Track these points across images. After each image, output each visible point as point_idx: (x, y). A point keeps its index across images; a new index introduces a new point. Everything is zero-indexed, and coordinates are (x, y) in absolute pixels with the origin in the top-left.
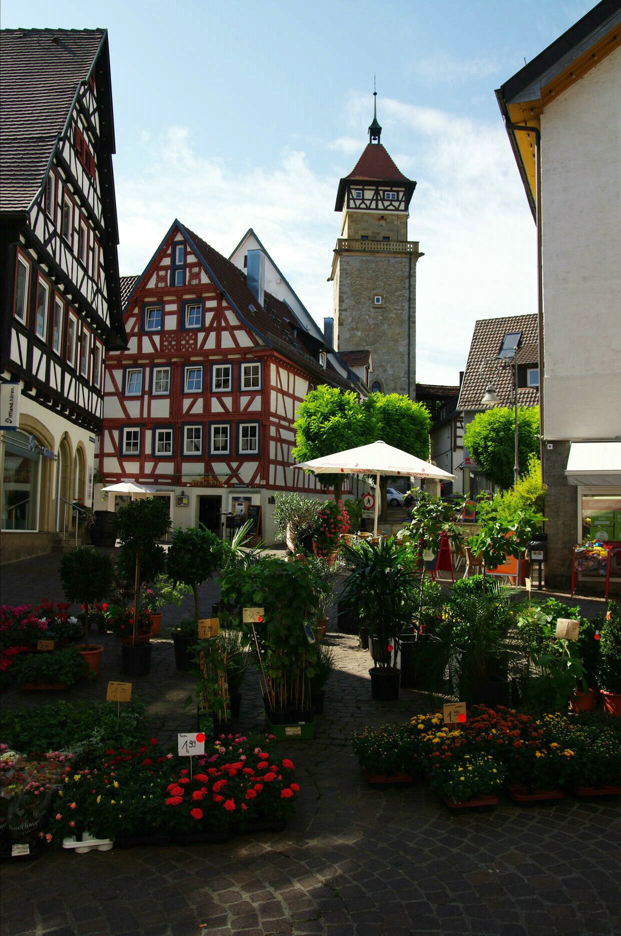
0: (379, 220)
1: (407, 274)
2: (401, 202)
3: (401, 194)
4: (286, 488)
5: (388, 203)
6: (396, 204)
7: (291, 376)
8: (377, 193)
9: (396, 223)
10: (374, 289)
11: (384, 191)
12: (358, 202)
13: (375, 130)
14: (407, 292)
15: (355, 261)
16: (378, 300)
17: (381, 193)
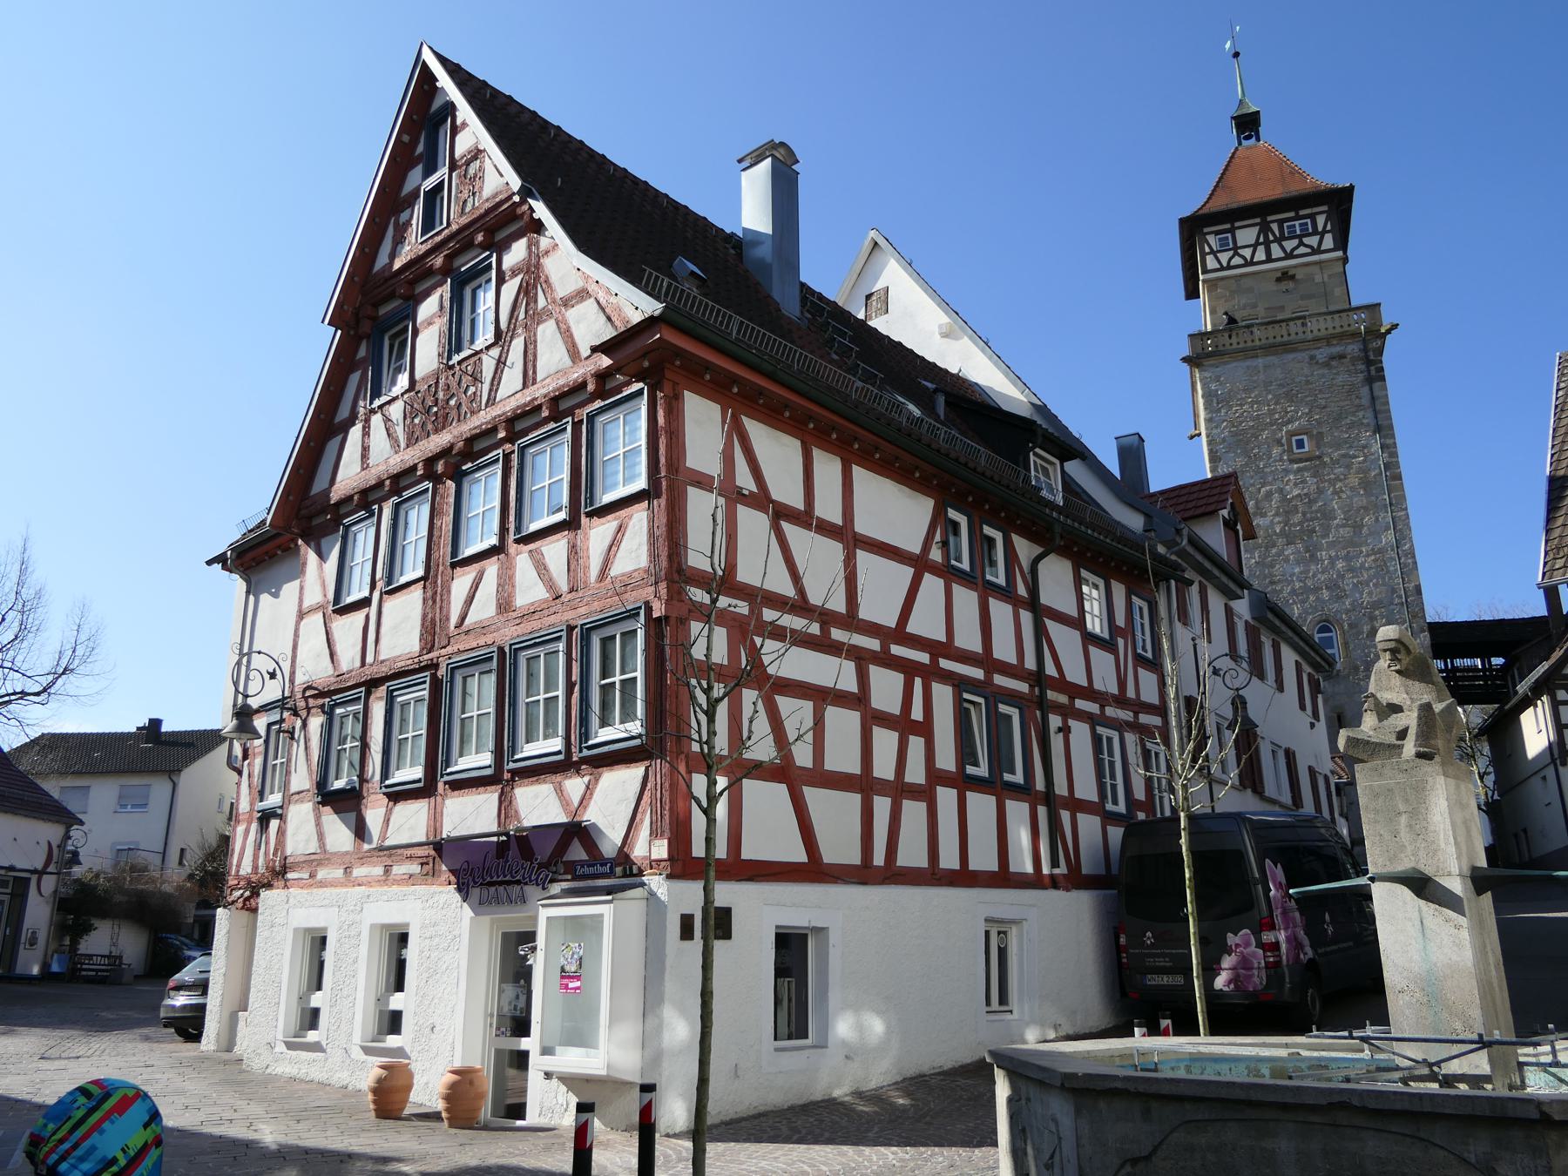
0: (1278, 280)
2: (1324, 232)
3: (1321, 220)
4: (814, 870)
5: (1295, 242)
6: (1313, 241)
7: (828, 468)
8: (1265, 228)
9: (1318, 279)
10: (1289, 422)
11: (1281, 222)
12: (1224, 258)
13: (1247, 124)
14: (1370, 414)
15: (1235, 373)
16: (1300, 444)
17: (1275, 227)
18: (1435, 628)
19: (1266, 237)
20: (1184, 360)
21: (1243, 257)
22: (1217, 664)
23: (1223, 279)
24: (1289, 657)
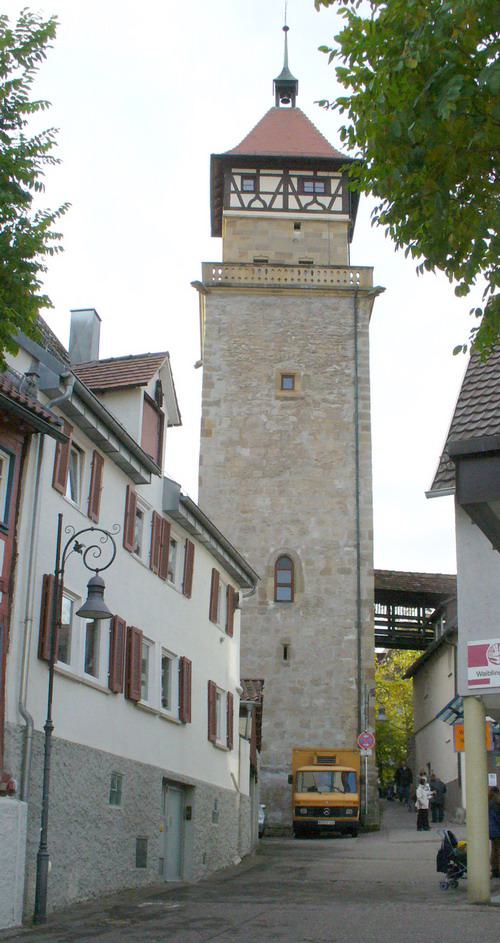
1: (349, 330)
5: (310, 199)
6: (325, 201)
8: (286, 180)
9: (325, 235)
11: (302, 180)
12: (247, 198)
15: (238, 307)
17: (294, 181)
18: (380, 575)
19: (286, 189)
20: (195, 284)
21: (264, 202)
22: (80, 539)
23: (242, 218)
24: (204, 565)
